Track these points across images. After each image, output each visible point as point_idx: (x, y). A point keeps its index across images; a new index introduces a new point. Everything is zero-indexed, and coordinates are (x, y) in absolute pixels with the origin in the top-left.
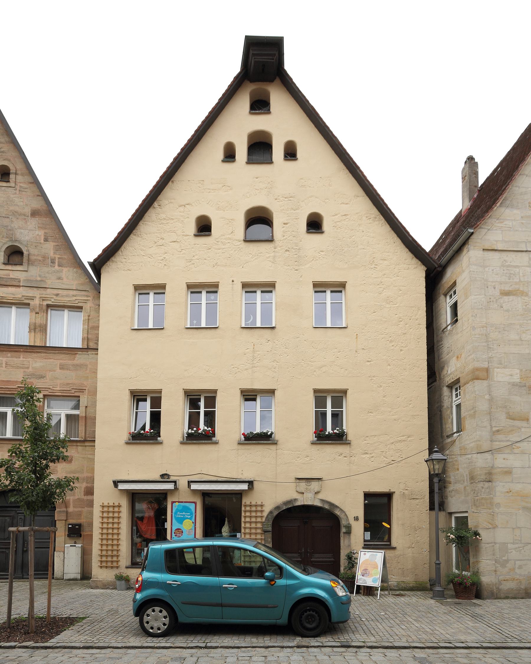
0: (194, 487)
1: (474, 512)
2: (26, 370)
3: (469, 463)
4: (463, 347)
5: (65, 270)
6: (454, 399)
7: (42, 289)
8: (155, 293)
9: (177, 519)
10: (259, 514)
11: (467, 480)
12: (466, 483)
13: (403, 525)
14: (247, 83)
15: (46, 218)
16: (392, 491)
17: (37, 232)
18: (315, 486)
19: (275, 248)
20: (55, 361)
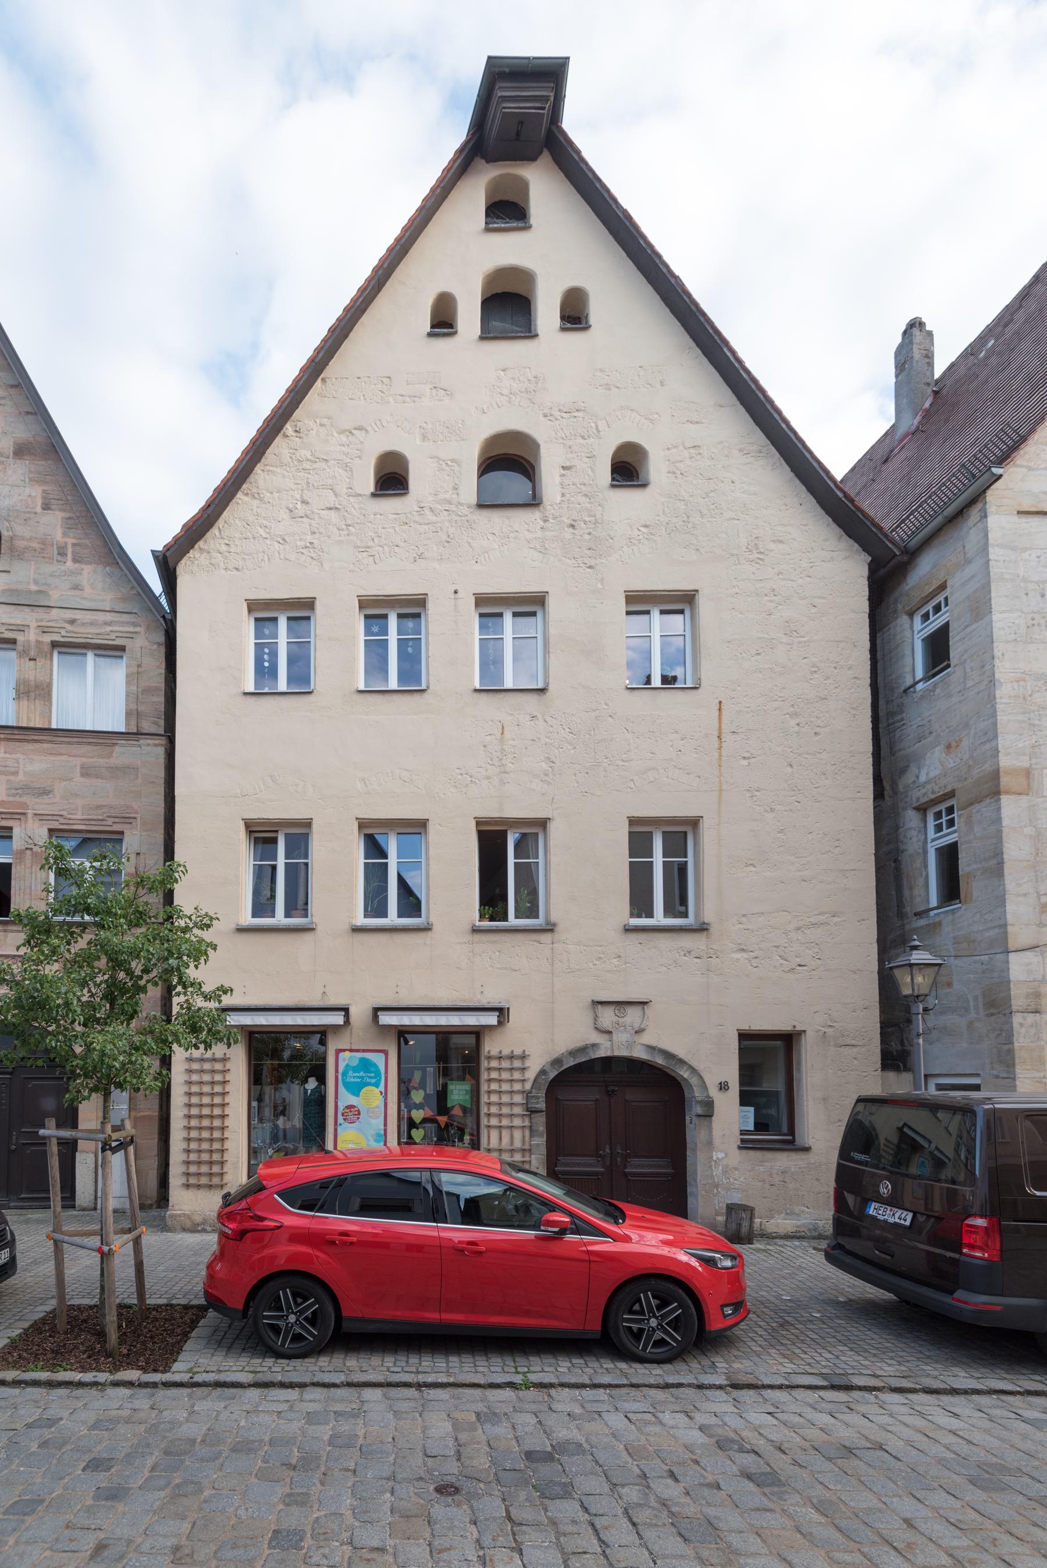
0: (386, 1019)
1: (997, 1077)
2: (12, 778)
3: (983, 972)
4: (967, 725)
5: (87, 569)
6: (931, 833)
7: (40, 610)
8: (289, 619)
9: (347, 1086)
10: (517, 1075)
11: (976, 1008)
12: (973, 1015)
13: (824, 1099)
14: (479, 163)
15: (46, 460)
16: (798, 1028)
17: (28, 491)
18: (633, 1016)
19: (546, 521)
20: (71, 759)
